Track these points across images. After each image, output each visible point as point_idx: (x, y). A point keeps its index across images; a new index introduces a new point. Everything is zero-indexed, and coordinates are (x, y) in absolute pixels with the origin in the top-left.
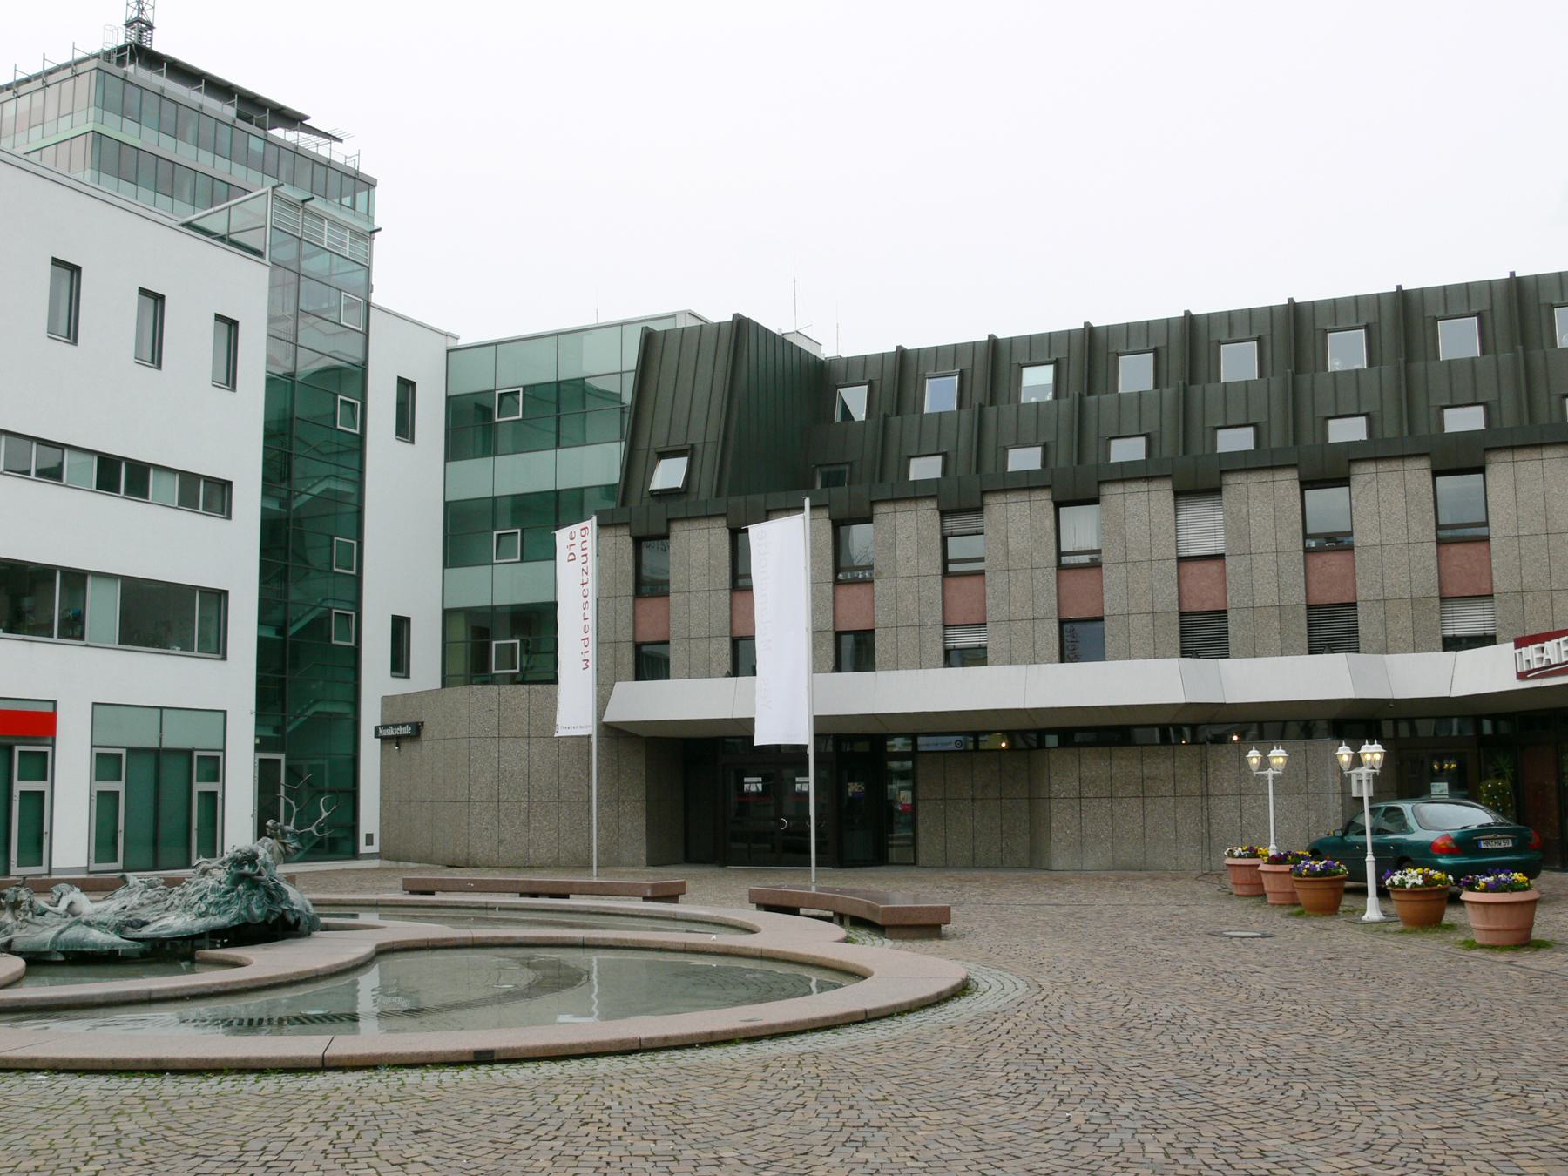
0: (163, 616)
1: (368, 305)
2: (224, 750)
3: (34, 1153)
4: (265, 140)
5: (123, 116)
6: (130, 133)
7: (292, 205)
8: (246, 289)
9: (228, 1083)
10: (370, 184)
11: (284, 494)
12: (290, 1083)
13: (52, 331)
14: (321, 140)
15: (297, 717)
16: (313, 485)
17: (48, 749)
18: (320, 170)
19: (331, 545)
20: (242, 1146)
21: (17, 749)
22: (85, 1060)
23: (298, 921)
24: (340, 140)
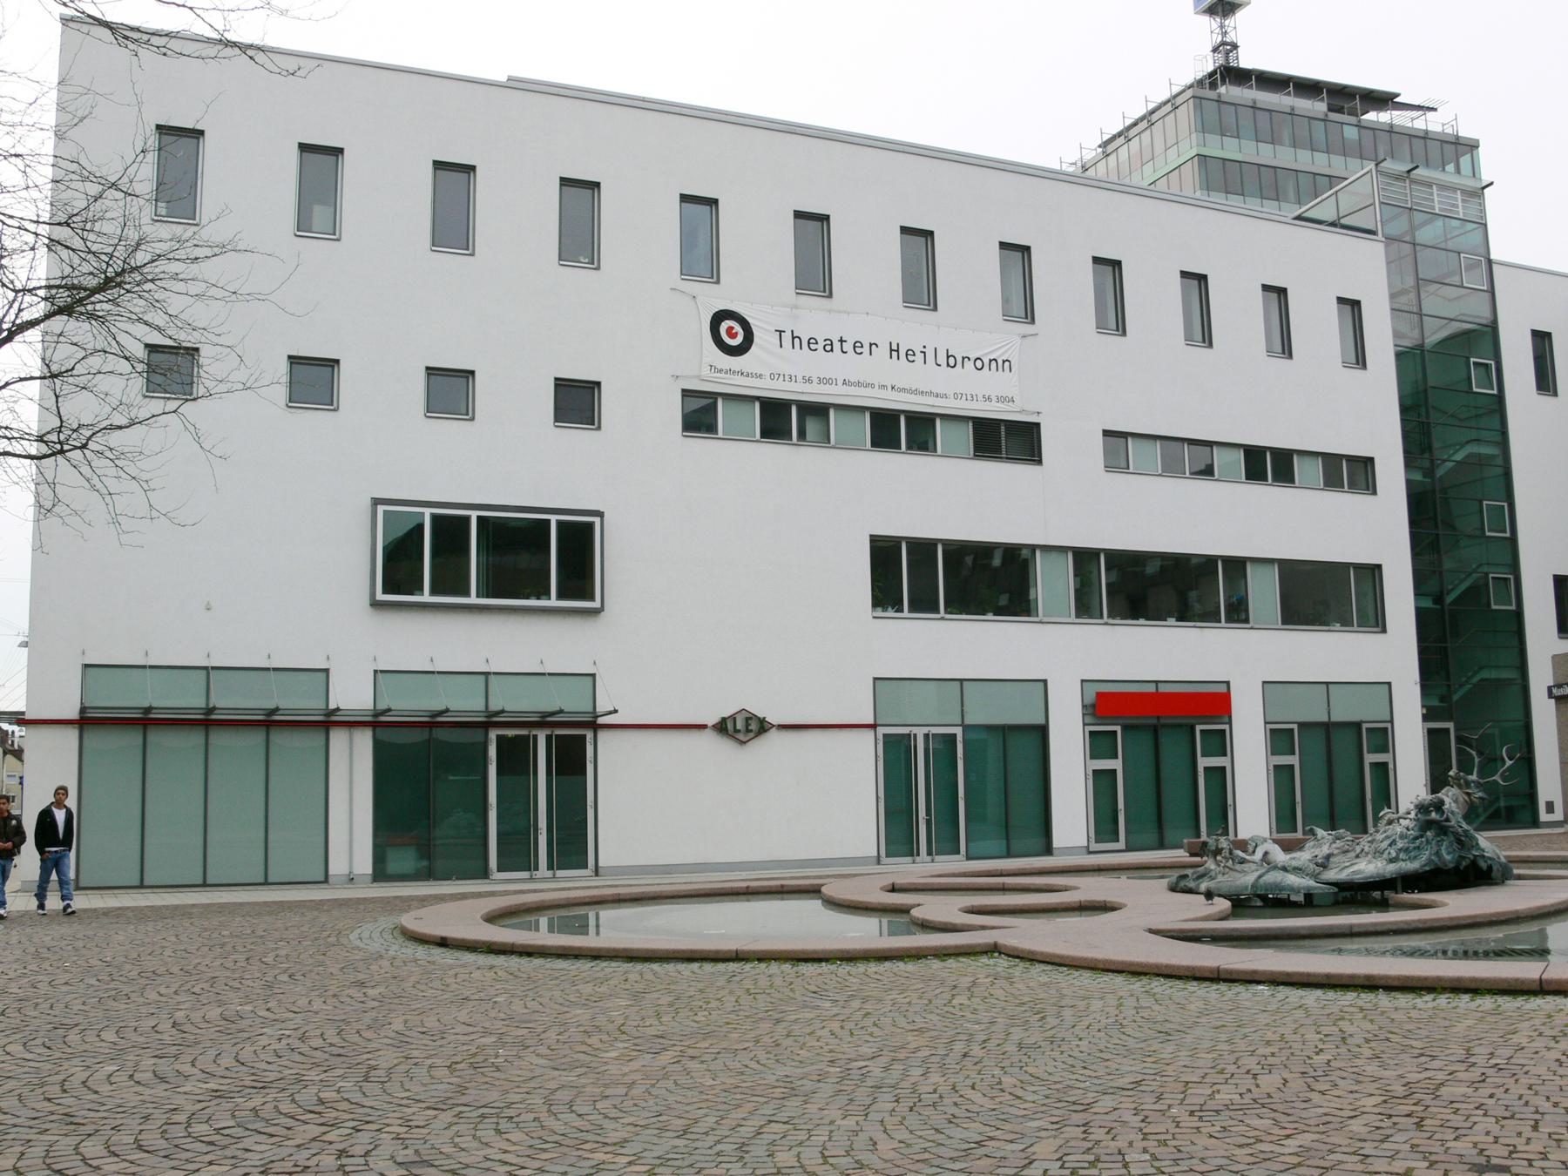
0: (1322, 594)
1: (1490, 262)
2: (1392, 722)
3: (1268, 1043)
4: (1359, 126)
5: (1222, 135)
6: (1231, 149)
7: (1398, 178)
8: (1364, 268)
9: (1443, 1000)
10: (1472, 146)
11: (1426, 464)
12: (1507, 1003)
13: (1189, 338)
14: (1415, 114)
15: (1462, 686)
16: (1454, 454)
17: (1226, 727)
18: (1418, 143)
19: (1481, 511)
20: (1468, 1050)
21: (1198, 728)
22: (1301, 974)
23: (1490, 868)
24: (1434, 109)
